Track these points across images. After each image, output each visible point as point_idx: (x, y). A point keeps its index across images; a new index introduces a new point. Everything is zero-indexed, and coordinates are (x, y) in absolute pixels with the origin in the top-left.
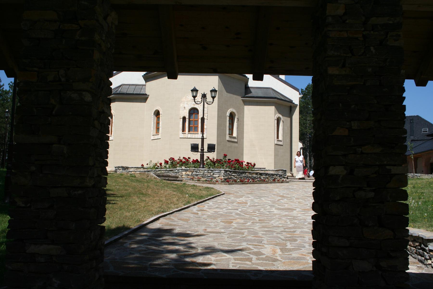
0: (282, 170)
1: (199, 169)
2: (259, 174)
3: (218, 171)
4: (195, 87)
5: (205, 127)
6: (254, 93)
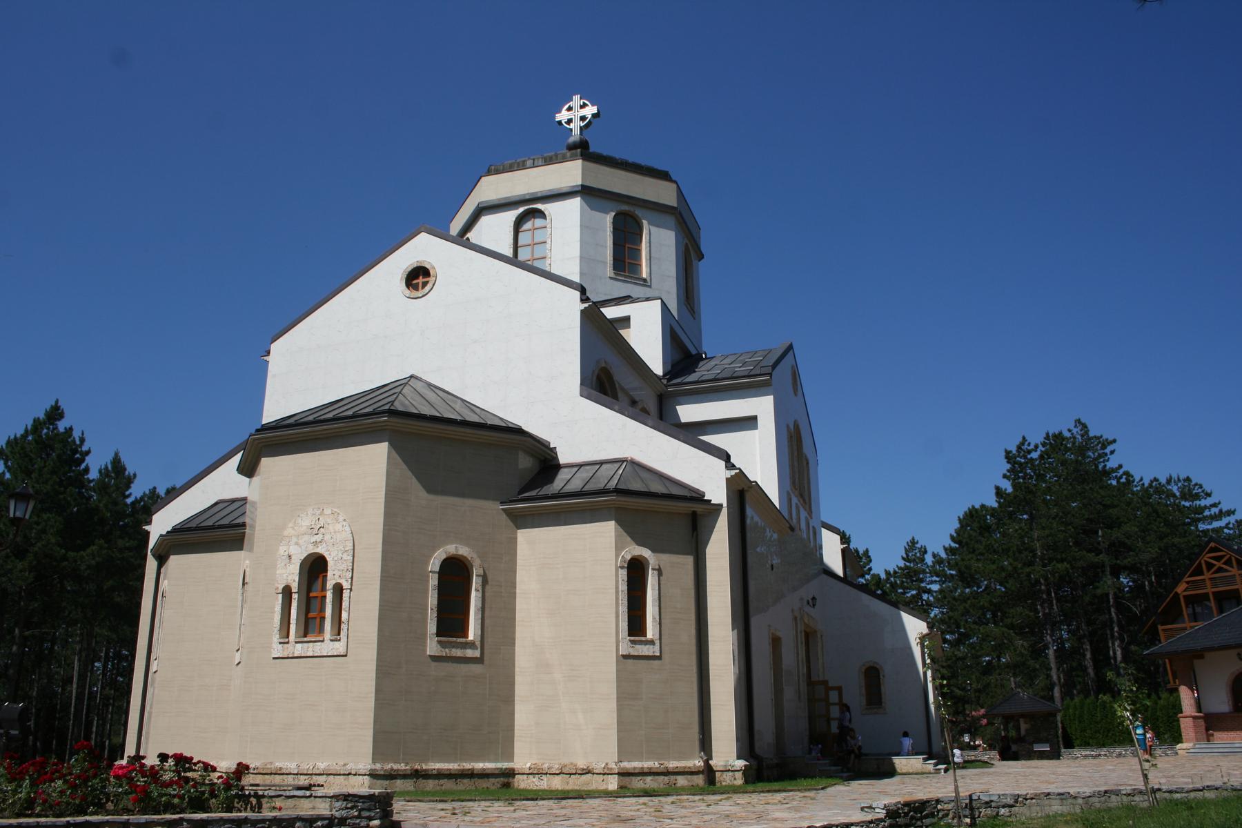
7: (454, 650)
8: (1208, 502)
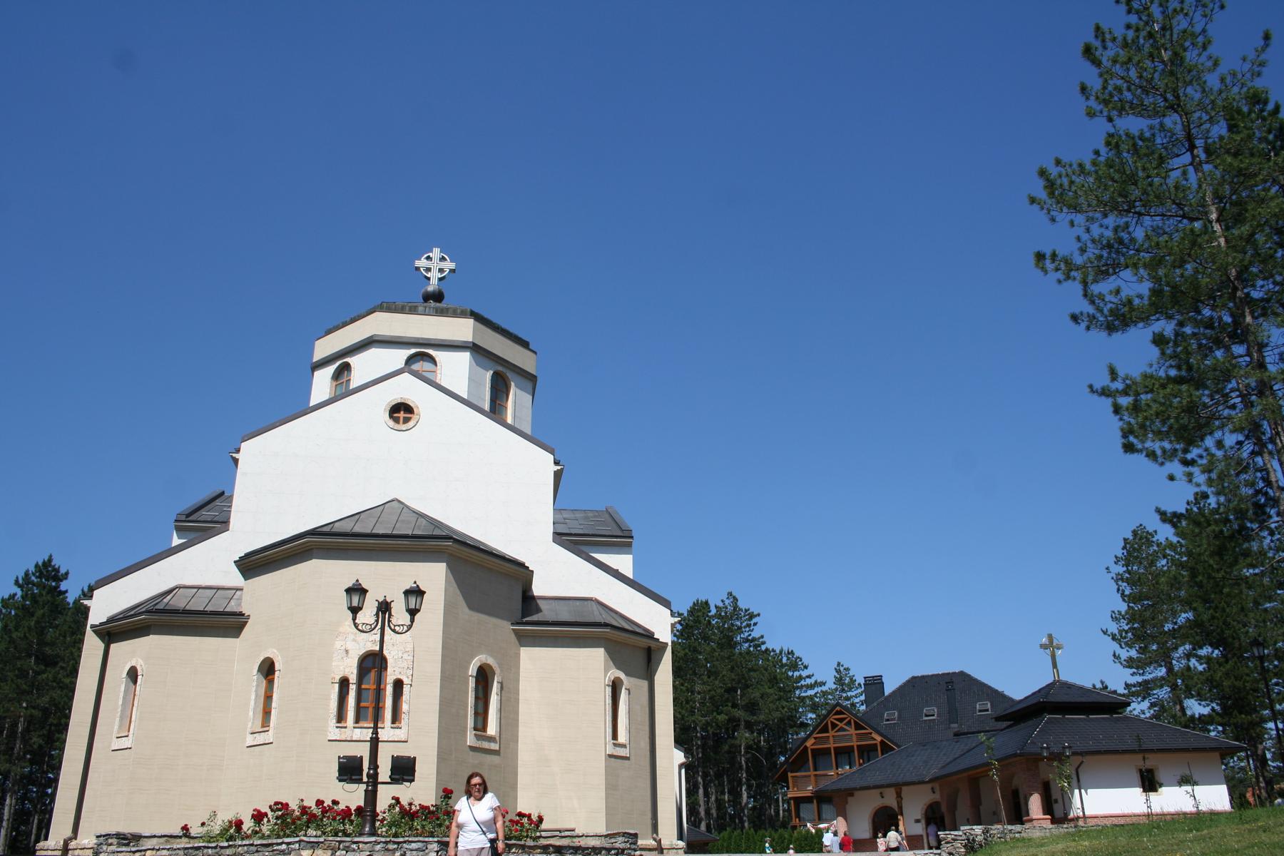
0: (624, 834)
1: (356, 839)
2: (551, 849)
3: (420, 845)
4: (357, 581)
5: (405, 707)
6: (546, 613)
7: (484, 742)
8: (804, 673)
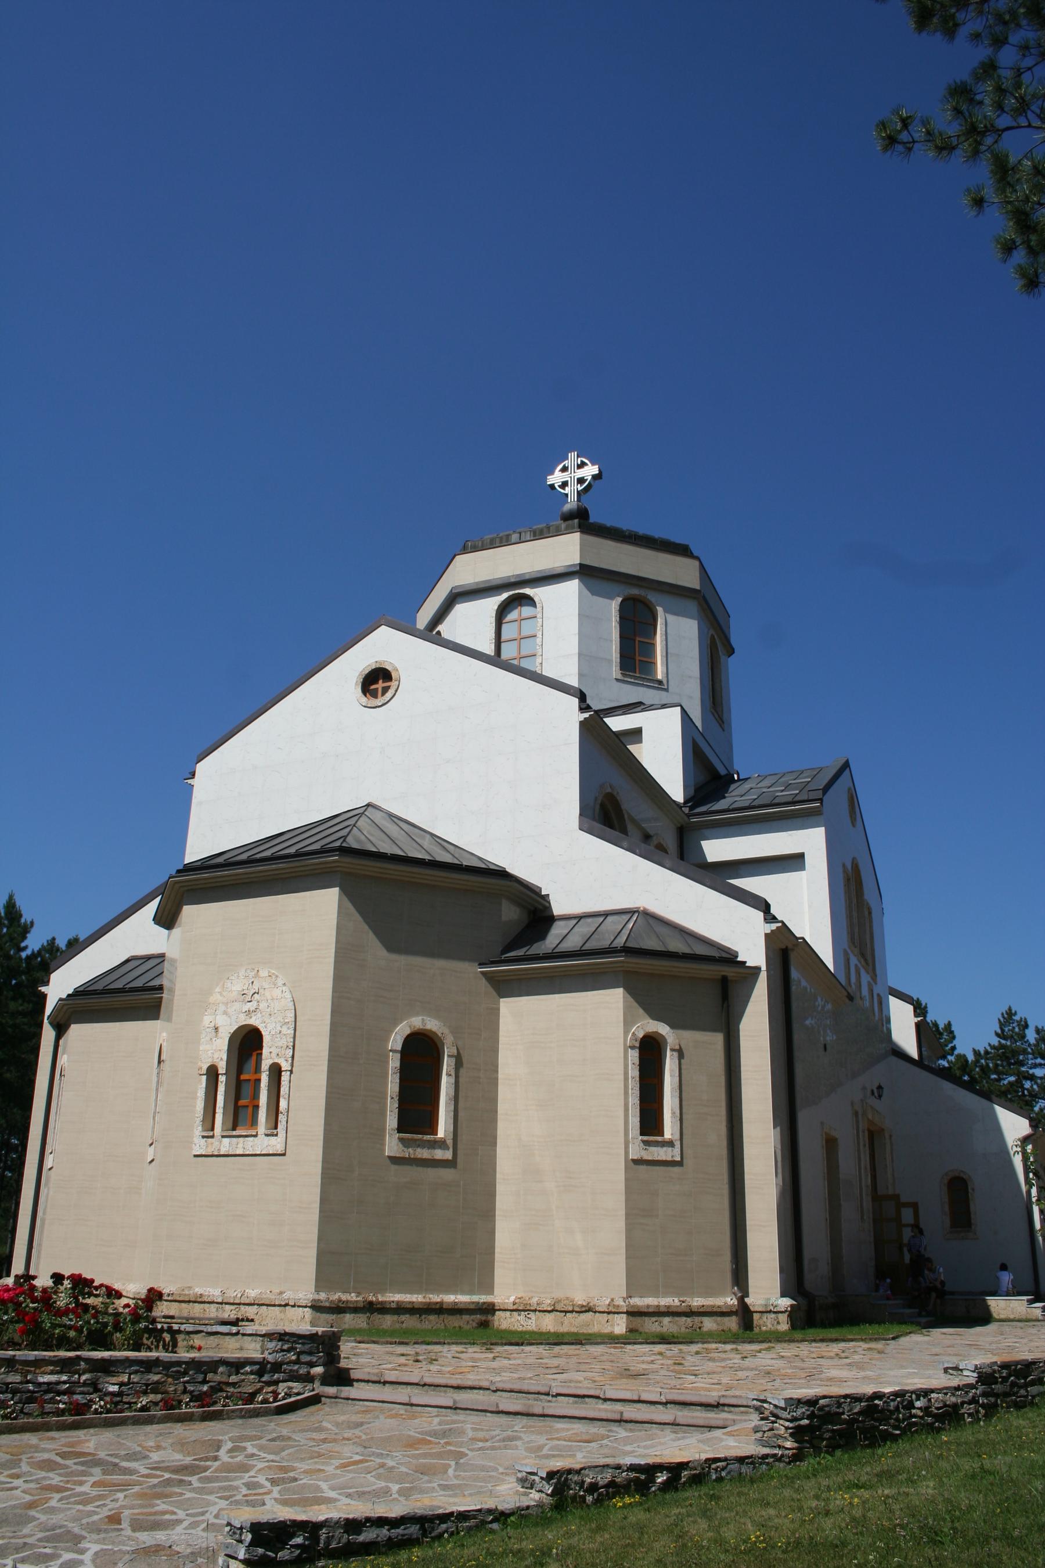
7: (419, 1150)
